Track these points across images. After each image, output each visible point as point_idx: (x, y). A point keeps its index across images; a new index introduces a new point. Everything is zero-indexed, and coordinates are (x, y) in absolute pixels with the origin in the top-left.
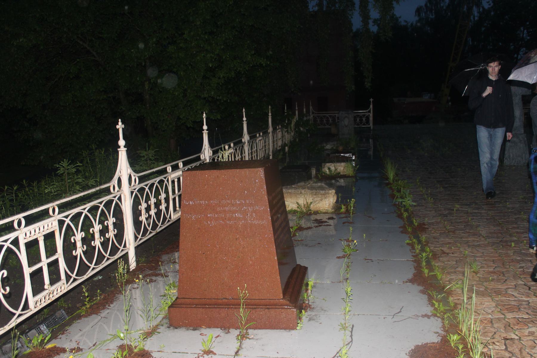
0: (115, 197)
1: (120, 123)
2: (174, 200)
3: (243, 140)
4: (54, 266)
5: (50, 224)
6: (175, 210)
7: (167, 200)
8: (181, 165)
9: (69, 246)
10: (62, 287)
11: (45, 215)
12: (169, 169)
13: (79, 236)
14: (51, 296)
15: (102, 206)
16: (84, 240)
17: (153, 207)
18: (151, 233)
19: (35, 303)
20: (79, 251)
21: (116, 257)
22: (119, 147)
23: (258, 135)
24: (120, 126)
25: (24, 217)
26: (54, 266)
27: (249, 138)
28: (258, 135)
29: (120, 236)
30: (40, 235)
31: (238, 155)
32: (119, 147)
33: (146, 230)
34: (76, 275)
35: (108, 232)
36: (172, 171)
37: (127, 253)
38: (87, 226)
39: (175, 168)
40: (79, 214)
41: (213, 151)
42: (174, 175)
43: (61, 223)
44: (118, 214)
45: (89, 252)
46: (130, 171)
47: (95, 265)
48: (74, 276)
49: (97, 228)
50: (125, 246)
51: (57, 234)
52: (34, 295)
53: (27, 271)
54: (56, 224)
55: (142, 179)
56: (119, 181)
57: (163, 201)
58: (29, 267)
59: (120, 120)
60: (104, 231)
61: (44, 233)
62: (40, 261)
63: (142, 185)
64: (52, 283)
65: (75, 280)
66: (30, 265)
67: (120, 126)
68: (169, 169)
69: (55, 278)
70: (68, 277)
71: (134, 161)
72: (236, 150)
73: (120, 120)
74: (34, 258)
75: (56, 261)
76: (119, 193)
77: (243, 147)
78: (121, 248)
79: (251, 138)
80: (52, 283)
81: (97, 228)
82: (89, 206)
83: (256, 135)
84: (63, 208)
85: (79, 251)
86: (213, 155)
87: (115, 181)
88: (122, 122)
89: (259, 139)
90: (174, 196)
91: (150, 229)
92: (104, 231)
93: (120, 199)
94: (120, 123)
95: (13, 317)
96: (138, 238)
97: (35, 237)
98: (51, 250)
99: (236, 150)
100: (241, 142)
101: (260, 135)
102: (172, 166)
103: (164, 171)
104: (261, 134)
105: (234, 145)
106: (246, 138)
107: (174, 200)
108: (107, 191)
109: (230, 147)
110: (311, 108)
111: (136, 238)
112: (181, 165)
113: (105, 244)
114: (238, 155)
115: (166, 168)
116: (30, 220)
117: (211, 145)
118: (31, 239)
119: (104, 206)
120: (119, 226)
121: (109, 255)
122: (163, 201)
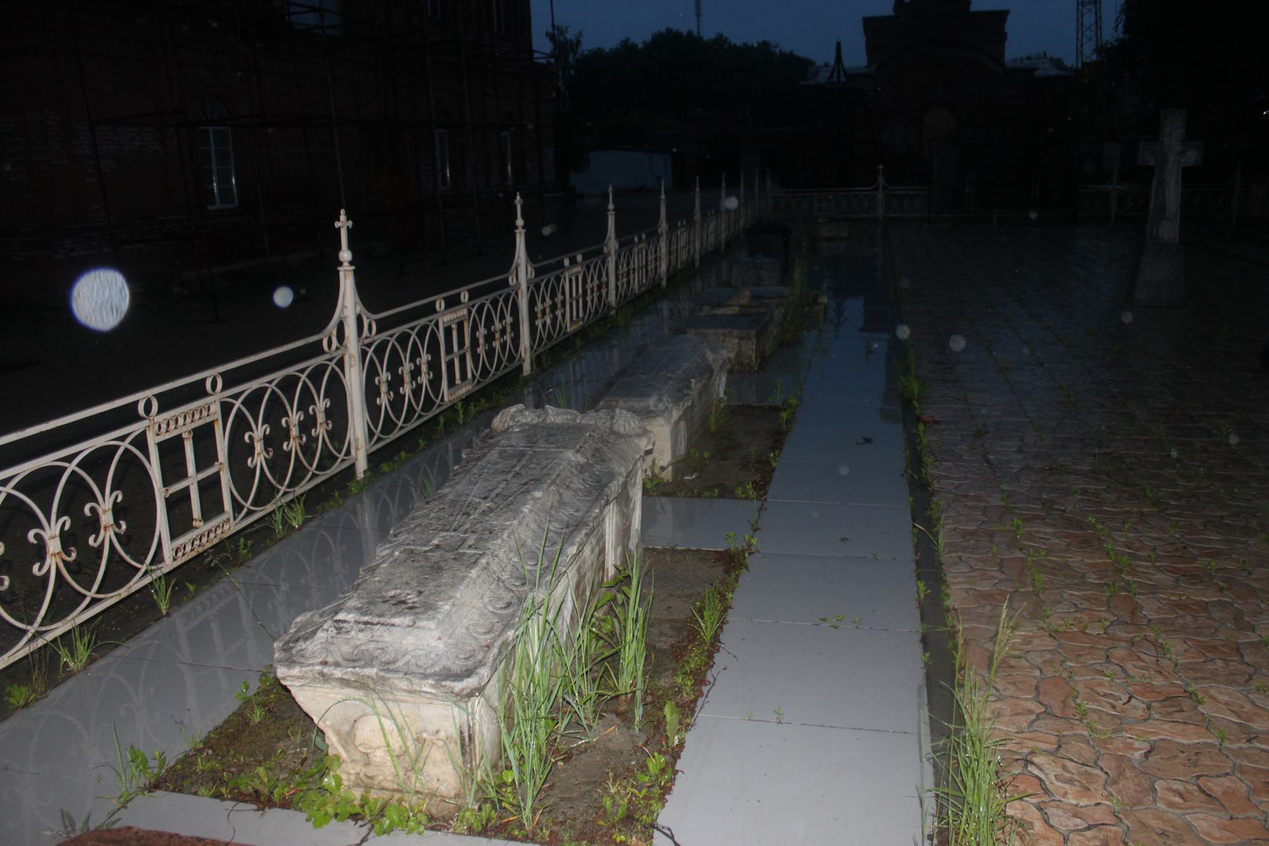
0: (330, 360)
1: (343, 218)
2: (450, 365)
3: (605, 250)
4: (210, 488)
5: (211, 406)
6: (452, 383)
7: (563, 303)
8: (465, 297)
9: (240, 451)
10: (228, 524)
11: (197, 391)
12: (440, 305)
13: (259, 431)
14: (212, 535)
15: (303, 377)
16: (268, 441)
17: (407, 378)
18: (420, 416)
19: (172, 550)
20: (259, 459)
21: (269, 508)
22: (341, 264)
23: (636, 239)
24: (343, 223)
25: (156, 396)
26: (210, 488)
27: (532, 274)
28: (636, 239)
29: (339, 431)
30: (185, 428)
31: (592, 280)
32: (341, 264)
33: (411, 410)
34: (252, 504)
35: (315, 426)
36: (446, 308)
37: (353, 465)
38: (276, 412)
39: (452, 302)
40: (260, 392)
41: (536, 269)
42: (446, 318)
43: (226, 408)
44: (337, 392)
45: (278, 463)
46: (360, 308)
47: (98, 592)
48: (248, 505)
49: (294, 418)
50: (348, 453)
51: (218, 428)
52: (174, 536)
53: (160, 494)
54: (216, 408)
55: (383, 326)
56: (341, 327)
57: (481, 341)
58: (165, 485)
59: (342, 211)
60: (308, 424)
61: (193, 426)
62: (185, 475)
63: (384, 336)
64: (206, 517)
65: (250, 513)
66: (167, 483)
67: (343, 223)
68: (440, 305)
69: (212, 507)
70: (237, 507)
71: (368, 295)
72: (588, 268)
73: (342, 211)
74: (174, 469)
75: (216, 479)
76: (340, 352)
77: (604, 262)
78: (438, 401)
79: (621, 245)
80: (206, 517)
81: (294, 418)
82: (279, 375)
83: (562, 261)
84: (231, 379)
85: (259, 459)
86: (536, 276)
87: (332, 328)
88: (347, 214)
89: (639, 249)
90: (450, 357)
91: (419, 409)
92: (308, 424)
93: (341, 363)
94: (343, 218)
95: (134, 575)
96: (242, 507)
97: (176, 433)
98: (206, 456)
99: (588, 268)
100: (600, 252)
101: (640, 239)
102: (469, 291)
103: (431, 309)
104: (644, 236)
105: (584, 258)
106: (612, 244)
107: (450, 365)
108: (316, 349)
109: (573, 262)
110: (769, 182)
111: (371, 434)
112: (465, 297)
113: (308, 450)
114: (592, 280)
115: (434, 302)
116: (168, 401)
117: (669, 219)
118: (168, 436)
119: (243, 403)
120: (338, 414)
121: (253, 504)
122: (481, 341)
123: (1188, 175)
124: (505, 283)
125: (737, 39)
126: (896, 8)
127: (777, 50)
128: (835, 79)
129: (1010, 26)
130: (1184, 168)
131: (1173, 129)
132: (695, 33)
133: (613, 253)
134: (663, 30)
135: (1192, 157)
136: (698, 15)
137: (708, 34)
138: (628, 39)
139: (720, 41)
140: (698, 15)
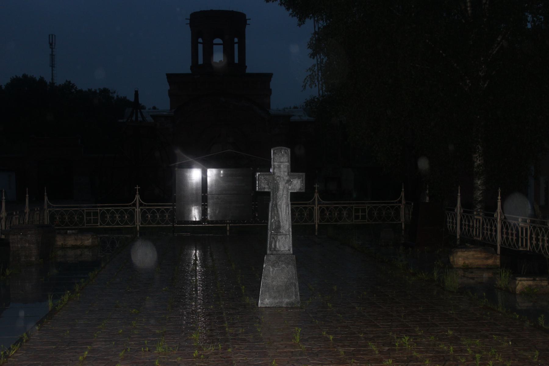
23: (14, 213)
28: (14, 213)
101: (16, 213)
123: (295, 197)
124: (493, 216)
125: (82, 85)
126: (192, 68)
127: (115, 96)
128: (134, 118)
129: (274, 84)
130: (292, 194)
131: (281, 162)
132: (48, 80)
133: (4, 218)
134: (20, 75)
135: (297, 185)
136: (53, 66)
137: (59, 81)
138: (126, 97)
139: (68, 86)
140: (53, 66)
